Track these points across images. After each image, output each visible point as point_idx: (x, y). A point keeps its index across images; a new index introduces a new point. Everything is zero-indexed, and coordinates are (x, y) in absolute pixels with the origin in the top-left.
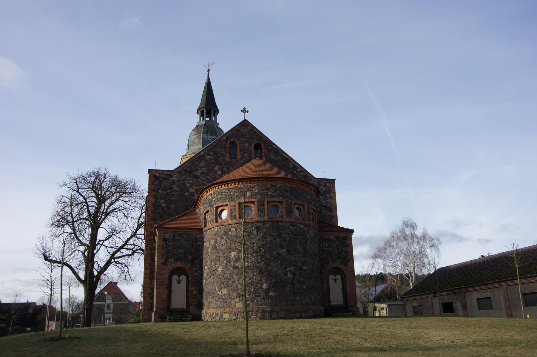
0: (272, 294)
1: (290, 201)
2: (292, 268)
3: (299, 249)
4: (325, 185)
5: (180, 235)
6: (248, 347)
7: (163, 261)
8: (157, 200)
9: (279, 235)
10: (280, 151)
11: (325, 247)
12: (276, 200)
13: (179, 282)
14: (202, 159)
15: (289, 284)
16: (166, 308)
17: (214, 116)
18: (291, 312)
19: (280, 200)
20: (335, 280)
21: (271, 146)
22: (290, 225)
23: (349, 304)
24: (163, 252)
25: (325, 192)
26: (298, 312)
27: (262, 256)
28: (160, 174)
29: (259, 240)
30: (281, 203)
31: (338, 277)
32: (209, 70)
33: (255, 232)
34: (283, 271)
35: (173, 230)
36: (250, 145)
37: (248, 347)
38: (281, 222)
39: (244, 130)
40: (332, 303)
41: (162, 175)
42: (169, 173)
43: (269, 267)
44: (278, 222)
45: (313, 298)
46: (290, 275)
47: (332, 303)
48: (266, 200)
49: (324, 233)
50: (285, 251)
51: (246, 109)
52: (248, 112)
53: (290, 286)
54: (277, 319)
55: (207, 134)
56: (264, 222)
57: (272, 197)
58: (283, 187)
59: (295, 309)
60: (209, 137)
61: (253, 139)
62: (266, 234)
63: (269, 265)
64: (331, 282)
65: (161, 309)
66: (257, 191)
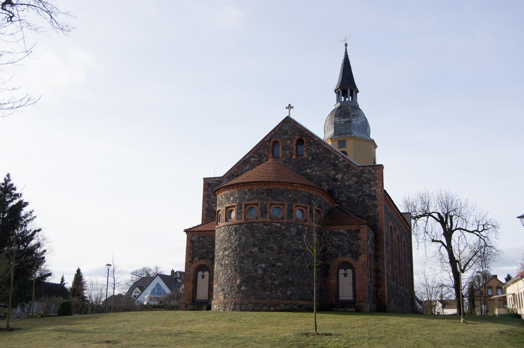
0: (243, 288)
1: (265, 202)
2: (263, 265)
3: (272, 247)
4: (370, 172)
5: (204, 237)
6: (8, 324)
7: (190, 259)
8: (209, 204)
9: (253, 235)
10: (322, 143)
11: (335, 241)
12: (252, 202)
13: (203, 277)
14: (247, 163)
15: (258, 279)
16: (191, 299)
18: (258, 306)
20: (345, 275)
21: (313, 139)
22: (264, 225)
23: (357, 299)
25: (370, 180)
26: (266, 306)
27: (237, 254)
28: (212, 181)
29: (236, 240)
30: (257, 204)
31: (349, 271)
32: (346, 45)
33: (234, 233)
34: (254, 268)
35: (198, 233)
36: (292, 142)
37: (8, 324)
38: (255, 223)
39: (286, 128)
40: (341, 298)
42: (219, 179)
43: (242, 265)
44: (252, 223)
45: (289, 293)
46: (260, 272)
47: (341, 298)
48: (243, 204)
49: (334, 227)
50: (256, 249)
51: (291, 106)
52: (293, 107)
53: (260, 281)
54: (245, 311)
55: (340, 117)
56: (241, 224)
57: (249, 200)
58: (259, 190)
59: (263, 303)
61: (295, 135)
62: (241, 234)
63: (243, 263)
64: (341, 276)
65: (187, 300)
66: (237, 196)
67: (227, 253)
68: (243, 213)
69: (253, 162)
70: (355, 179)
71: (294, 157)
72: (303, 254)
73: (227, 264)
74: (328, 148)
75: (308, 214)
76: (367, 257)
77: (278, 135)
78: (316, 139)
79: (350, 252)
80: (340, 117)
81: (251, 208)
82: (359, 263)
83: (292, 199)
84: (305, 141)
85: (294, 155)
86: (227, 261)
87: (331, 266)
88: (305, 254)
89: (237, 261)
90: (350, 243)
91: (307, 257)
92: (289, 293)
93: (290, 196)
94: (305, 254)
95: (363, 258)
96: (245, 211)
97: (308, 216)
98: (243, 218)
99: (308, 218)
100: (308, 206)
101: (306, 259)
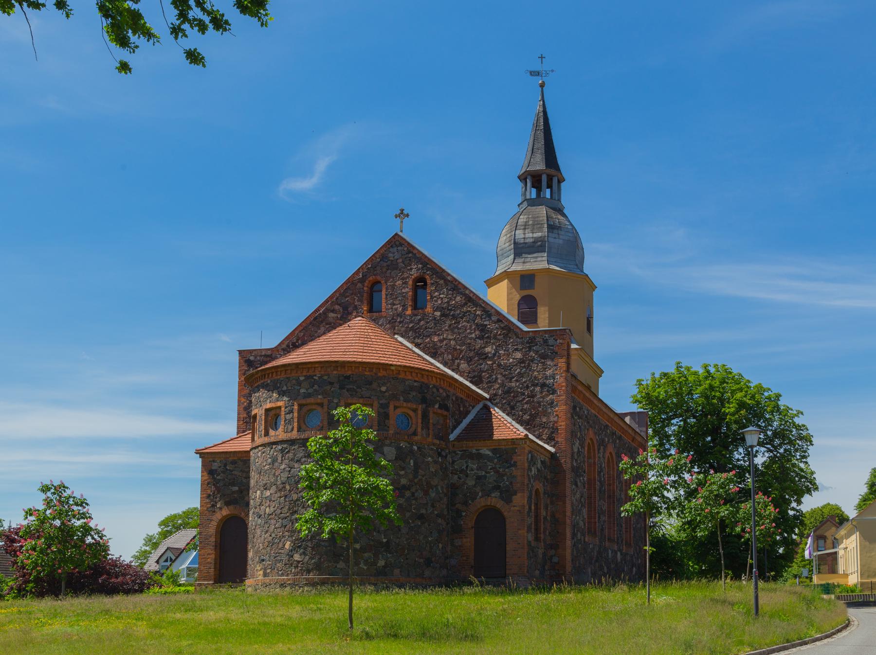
4: (545, 341)
10: (460, 286)
14: (322, 322)
17: (550, 186)
19: (319, 401)
24: (209, 491)
39: (394, 254)
41: (258, 358)
42: (269, 353)
52: (407, 215)
58: (326, 378)
60: (527, 236)
67: (268, 493)
68: (296, 420)
69: (331, 320)
70: (519, 355)
71: (409, 312)
72: (408, 494)
73: (269, 515)
74: (471, 295)
75: (420, 421)
76: (530, 498)
77: (378, 268)
78: (449, 278)
79: (497, 488)
80: (525, 229)
81: (310, 411)
82: (512, 508)
83: (387, 394)
84: (428, 281)
85: (410, 309)
86: (267, 509)
87: (464, 514)
88: (413, 494)
89: (285, 510)
90: (497, 472)
91: (416, 499)
92: (381, 563)
93: (384, 389)
94: (413, 494)
95: (520, 500)
96: (299, 418)
97: (420, 425)
98: (296, 429)
99: (419, 430)
100: (420, 408)
101: (414, 502)
